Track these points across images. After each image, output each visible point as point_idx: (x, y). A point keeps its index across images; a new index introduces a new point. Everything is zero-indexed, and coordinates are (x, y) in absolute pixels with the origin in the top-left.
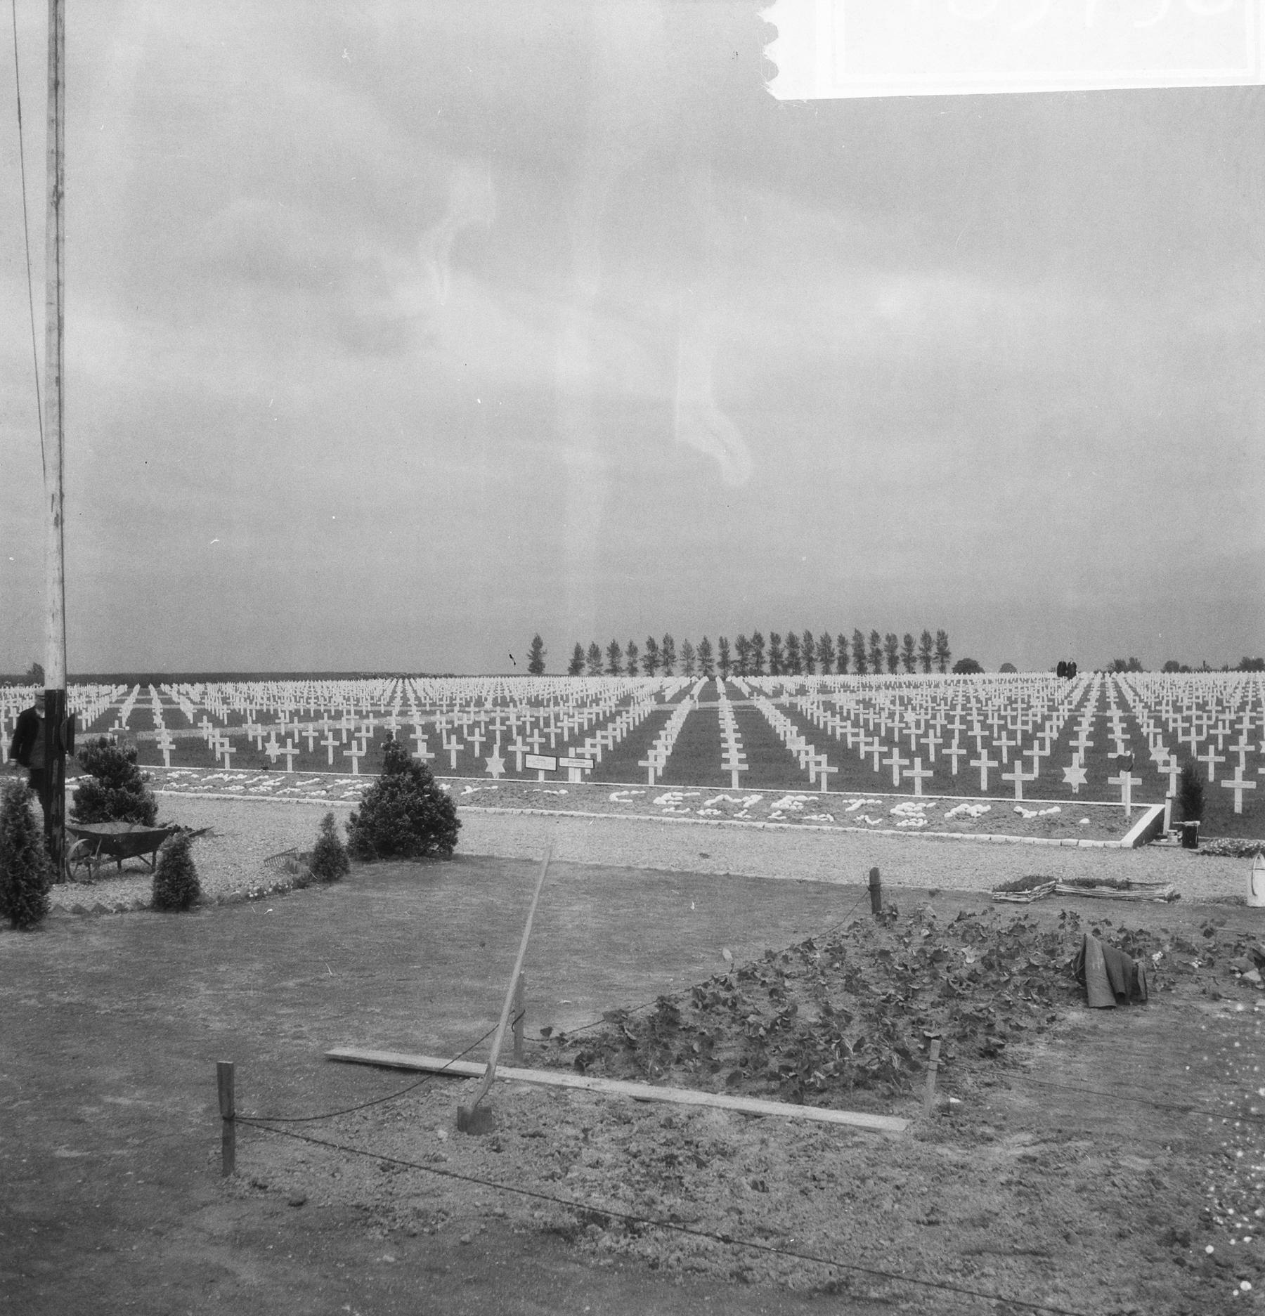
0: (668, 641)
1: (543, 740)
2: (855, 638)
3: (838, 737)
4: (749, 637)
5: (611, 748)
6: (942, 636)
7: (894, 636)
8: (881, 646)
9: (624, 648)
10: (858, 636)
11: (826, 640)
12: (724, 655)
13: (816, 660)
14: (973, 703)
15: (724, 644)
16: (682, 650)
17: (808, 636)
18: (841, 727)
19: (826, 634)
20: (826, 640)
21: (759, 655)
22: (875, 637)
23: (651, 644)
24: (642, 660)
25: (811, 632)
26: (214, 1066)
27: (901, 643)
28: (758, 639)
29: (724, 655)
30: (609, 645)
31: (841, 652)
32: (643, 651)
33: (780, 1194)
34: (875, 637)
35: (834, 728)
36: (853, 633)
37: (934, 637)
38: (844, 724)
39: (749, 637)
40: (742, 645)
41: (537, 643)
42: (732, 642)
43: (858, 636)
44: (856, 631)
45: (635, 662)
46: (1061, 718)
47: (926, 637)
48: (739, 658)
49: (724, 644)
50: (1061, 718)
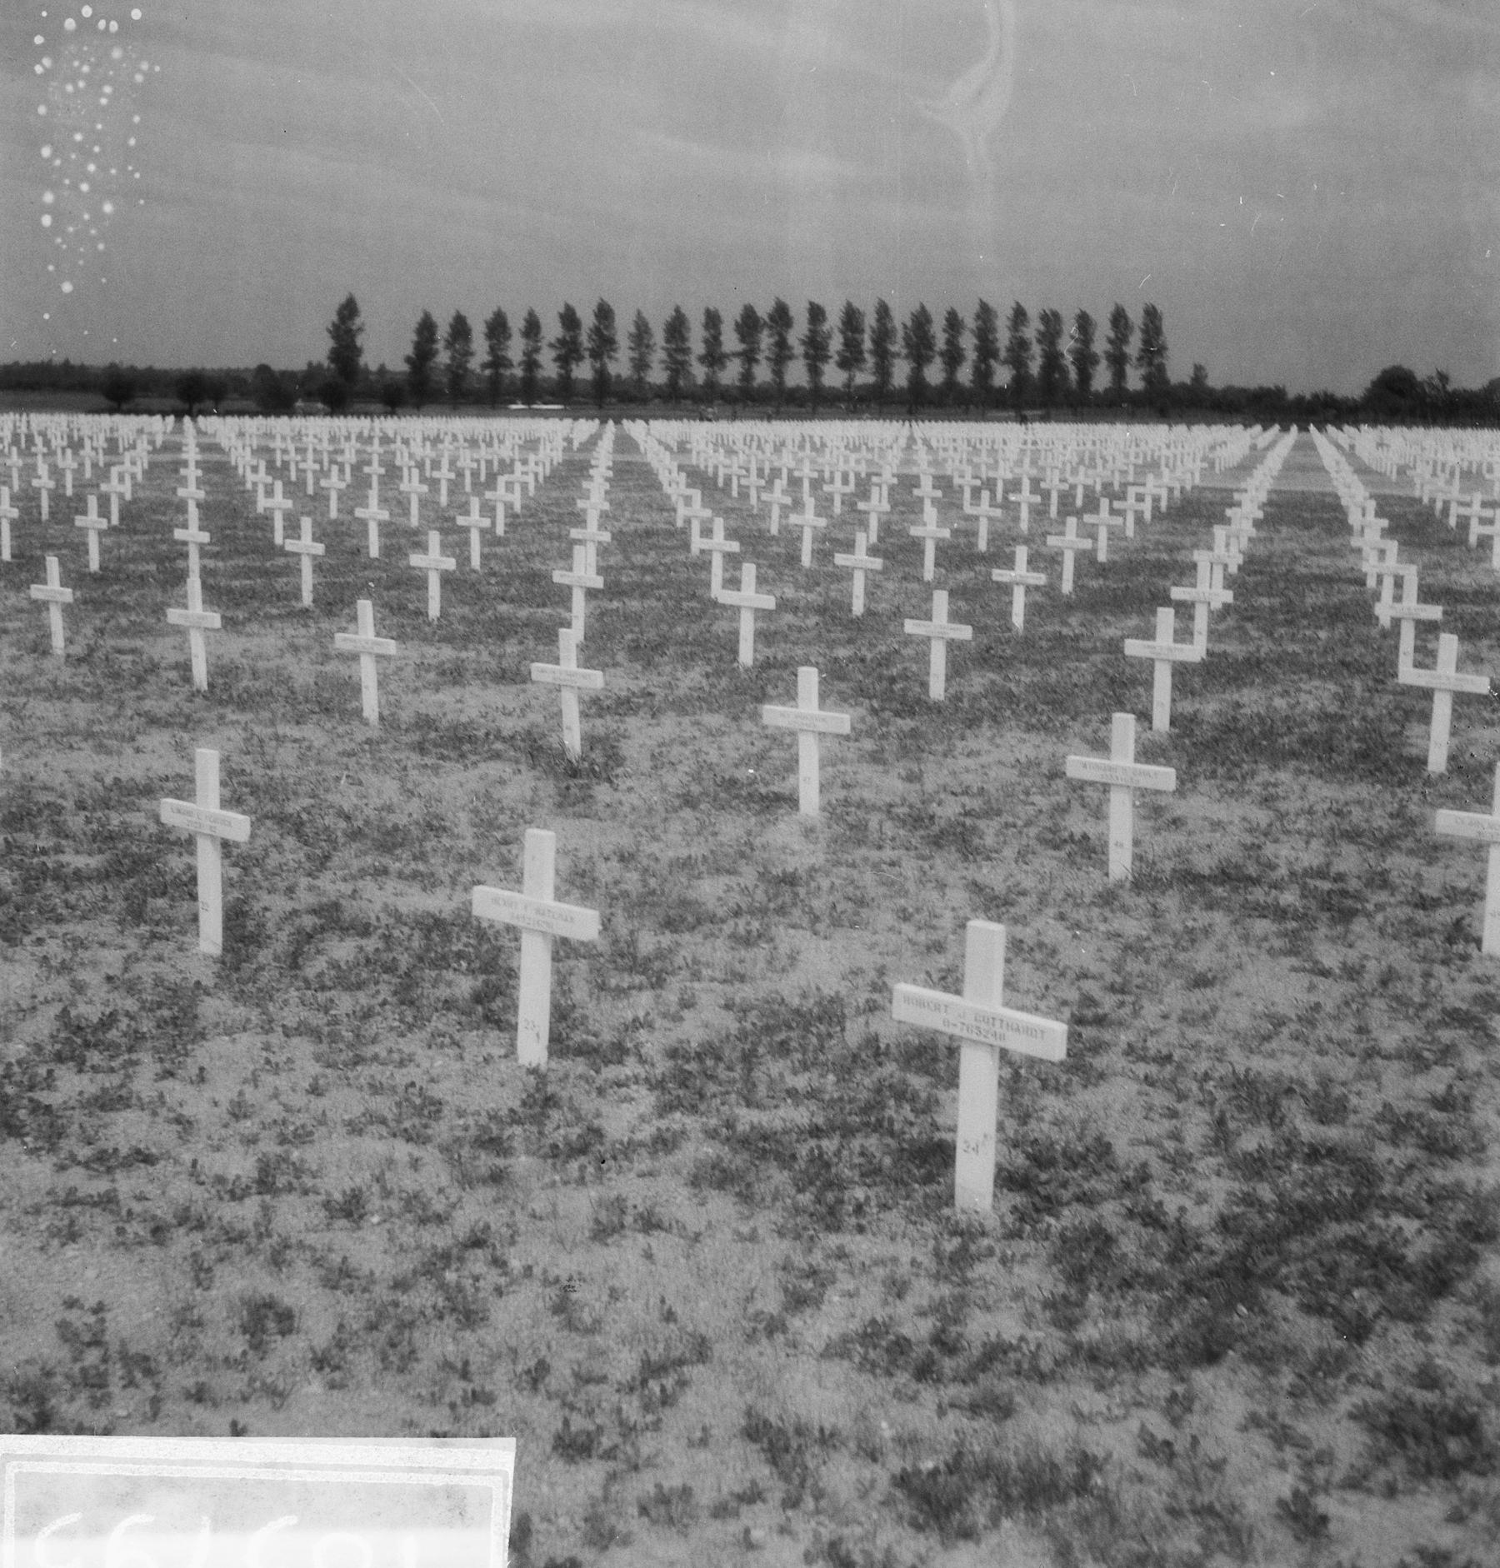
0: (604, 313)
1: (1038, 499)
2: (978, 317)
3: (1452, 522)
4: (764, 310)
5: (518, 508)
6: (1152, 314)
7: (1056, 315)
8: (1031, 331)
9: (516, 324)
10: (985, 313)
11: (921, 320)
12: (713, 342)
13: (898, 355)
14: (39, 447)
15: (712, 320)
16: (633, 329)
17: (883, 312)
18: (1461, 504)
19: (923, 308)
20: (921, 320)
21: (782, 344)
22: (1019, 315)
23: (569, 319)
24: (551, 345)
25: (891, 305)
26: (1345, 1423)
27: (1070, 329)
28: (781, 316)
29: (713, 342)
30: (489, 315)
31: (949, 342)
32: (552, 330)
33: (483, 1421)
34: (1019, 315)
35: (1446, 504)
36: (976, 308)
37: (1136, 317)
38: (1467, 498)
39: (764, 310)
40: (749, 324)
41: (349, 310)
42: (730, 316)
43: (985, 313)
44: (677, 310)
45: (537, 350)
46: (127, 478)
47: (1119, 319)
48: (740, 347)
49: (712, 320)
50: (127, 478)
